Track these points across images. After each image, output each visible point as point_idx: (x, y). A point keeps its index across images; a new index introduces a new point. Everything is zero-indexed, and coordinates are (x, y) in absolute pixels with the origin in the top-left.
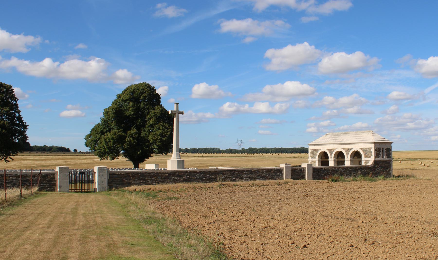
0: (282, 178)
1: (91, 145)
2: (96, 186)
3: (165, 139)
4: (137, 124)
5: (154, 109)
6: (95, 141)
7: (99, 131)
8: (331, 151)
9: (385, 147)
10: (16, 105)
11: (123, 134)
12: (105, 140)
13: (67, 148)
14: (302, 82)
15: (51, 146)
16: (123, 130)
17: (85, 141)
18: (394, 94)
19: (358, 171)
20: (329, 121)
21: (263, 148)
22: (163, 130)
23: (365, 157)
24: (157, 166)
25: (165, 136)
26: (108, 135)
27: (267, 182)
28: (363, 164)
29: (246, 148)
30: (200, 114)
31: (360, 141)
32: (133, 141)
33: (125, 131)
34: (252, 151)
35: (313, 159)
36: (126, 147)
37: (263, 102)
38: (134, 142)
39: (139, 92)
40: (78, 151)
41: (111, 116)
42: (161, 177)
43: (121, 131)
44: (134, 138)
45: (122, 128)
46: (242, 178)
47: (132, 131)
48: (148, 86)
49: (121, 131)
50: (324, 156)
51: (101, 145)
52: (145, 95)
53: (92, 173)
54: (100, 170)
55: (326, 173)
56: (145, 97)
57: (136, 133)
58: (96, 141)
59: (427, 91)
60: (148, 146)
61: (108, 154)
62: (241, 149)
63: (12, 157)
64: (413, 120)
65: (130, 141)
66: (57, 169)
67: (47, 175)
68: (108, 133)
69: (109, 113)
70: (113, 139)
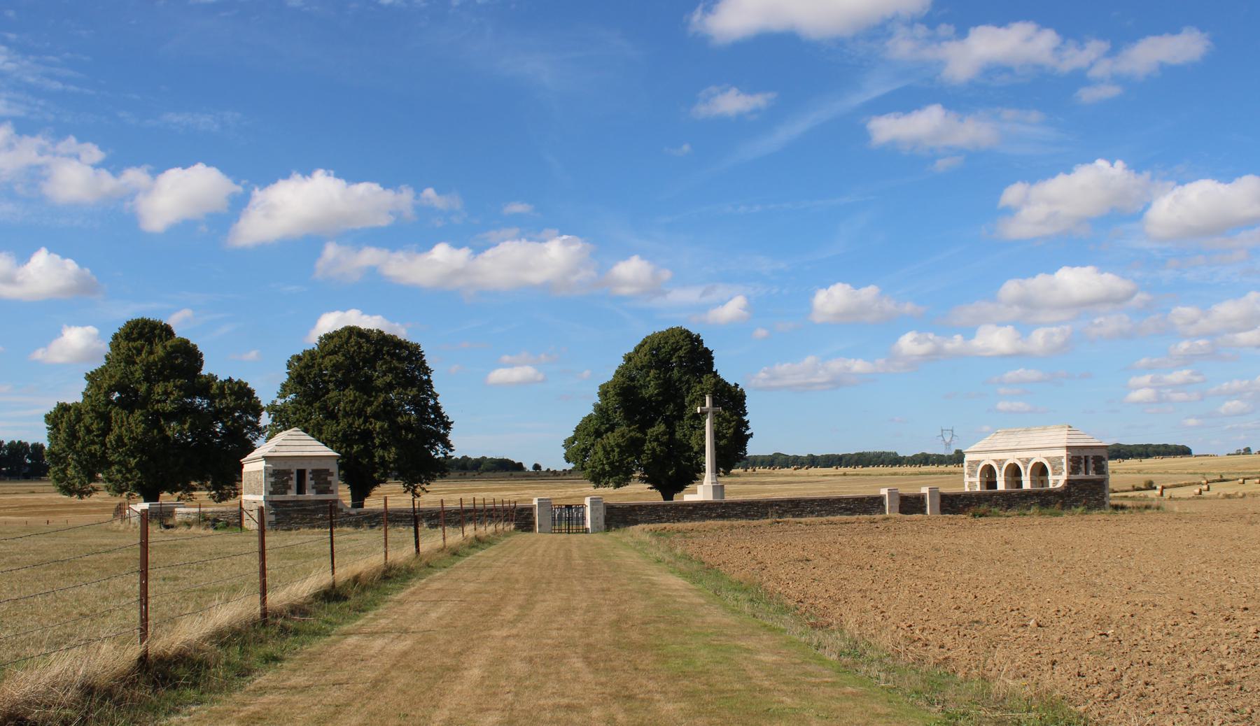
0: (883, 511)
2: (588, 525)
4: (666, 415)
5: (700, 382)
6: (583, 450)
8: (1000, 462)
9: (1091, 454)
10: (429, 382)
11: (639, 435)
12: (604, 448)
13: (516, 461)
14: (1102, 267)
15: (479, 456)
19: (1045, 500)
20: (1186, 372)
23: (1054, 474)
25: (724, 436)
27: (854, 518)
28: (1051, 486)
30: (836, 365)
31: (1043, 446)
32: (658, 449)
33: (643, 429)
35: (973, 479)
37: (1001, 324)
39: (668, 348)
40: (544, 469)
41: (613, 401)
42: (682, 511)
45: (636, 422)
46: (812, 512)
48: (688, 334)
50: (989, 472)
51: (596, 457)
52: (681, 353)
53: (583, 507)
54: (594, 502)
55: (965, 502)
56: (680, 357)
57: (664, 433)
58: (586, 450)
61: (611, 476)
62: (952, 452)
63: (424, 486)
65: (654, 449)
66: (535, 502)
67: (523, 510)
70: (618, 445)
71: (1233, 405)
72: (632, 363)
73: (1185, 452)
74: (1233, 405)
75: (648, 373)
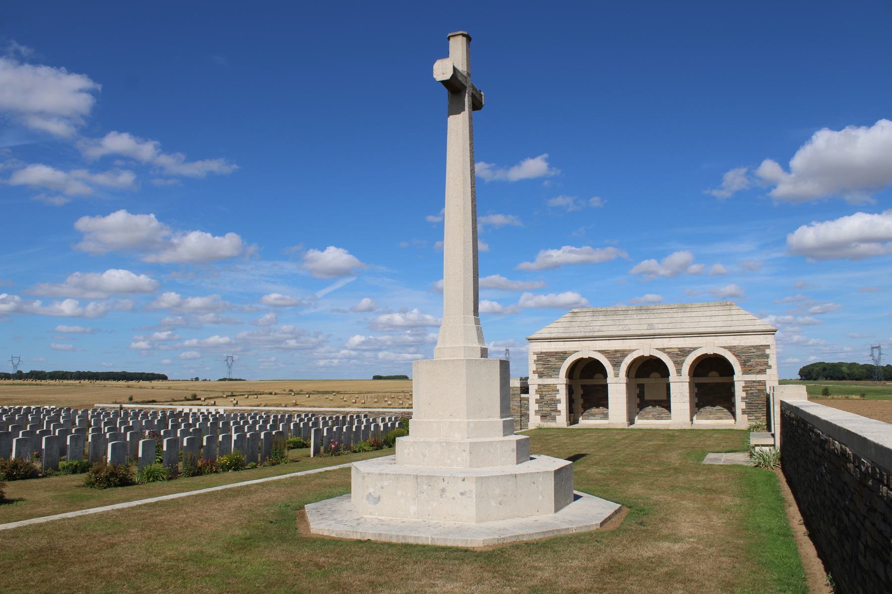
8: (616, 357)
23: (745, 372)
29: (26, 370)
59: (320, 294)
62: (15, 372)
64: (296, 335)
73: (164, 378)
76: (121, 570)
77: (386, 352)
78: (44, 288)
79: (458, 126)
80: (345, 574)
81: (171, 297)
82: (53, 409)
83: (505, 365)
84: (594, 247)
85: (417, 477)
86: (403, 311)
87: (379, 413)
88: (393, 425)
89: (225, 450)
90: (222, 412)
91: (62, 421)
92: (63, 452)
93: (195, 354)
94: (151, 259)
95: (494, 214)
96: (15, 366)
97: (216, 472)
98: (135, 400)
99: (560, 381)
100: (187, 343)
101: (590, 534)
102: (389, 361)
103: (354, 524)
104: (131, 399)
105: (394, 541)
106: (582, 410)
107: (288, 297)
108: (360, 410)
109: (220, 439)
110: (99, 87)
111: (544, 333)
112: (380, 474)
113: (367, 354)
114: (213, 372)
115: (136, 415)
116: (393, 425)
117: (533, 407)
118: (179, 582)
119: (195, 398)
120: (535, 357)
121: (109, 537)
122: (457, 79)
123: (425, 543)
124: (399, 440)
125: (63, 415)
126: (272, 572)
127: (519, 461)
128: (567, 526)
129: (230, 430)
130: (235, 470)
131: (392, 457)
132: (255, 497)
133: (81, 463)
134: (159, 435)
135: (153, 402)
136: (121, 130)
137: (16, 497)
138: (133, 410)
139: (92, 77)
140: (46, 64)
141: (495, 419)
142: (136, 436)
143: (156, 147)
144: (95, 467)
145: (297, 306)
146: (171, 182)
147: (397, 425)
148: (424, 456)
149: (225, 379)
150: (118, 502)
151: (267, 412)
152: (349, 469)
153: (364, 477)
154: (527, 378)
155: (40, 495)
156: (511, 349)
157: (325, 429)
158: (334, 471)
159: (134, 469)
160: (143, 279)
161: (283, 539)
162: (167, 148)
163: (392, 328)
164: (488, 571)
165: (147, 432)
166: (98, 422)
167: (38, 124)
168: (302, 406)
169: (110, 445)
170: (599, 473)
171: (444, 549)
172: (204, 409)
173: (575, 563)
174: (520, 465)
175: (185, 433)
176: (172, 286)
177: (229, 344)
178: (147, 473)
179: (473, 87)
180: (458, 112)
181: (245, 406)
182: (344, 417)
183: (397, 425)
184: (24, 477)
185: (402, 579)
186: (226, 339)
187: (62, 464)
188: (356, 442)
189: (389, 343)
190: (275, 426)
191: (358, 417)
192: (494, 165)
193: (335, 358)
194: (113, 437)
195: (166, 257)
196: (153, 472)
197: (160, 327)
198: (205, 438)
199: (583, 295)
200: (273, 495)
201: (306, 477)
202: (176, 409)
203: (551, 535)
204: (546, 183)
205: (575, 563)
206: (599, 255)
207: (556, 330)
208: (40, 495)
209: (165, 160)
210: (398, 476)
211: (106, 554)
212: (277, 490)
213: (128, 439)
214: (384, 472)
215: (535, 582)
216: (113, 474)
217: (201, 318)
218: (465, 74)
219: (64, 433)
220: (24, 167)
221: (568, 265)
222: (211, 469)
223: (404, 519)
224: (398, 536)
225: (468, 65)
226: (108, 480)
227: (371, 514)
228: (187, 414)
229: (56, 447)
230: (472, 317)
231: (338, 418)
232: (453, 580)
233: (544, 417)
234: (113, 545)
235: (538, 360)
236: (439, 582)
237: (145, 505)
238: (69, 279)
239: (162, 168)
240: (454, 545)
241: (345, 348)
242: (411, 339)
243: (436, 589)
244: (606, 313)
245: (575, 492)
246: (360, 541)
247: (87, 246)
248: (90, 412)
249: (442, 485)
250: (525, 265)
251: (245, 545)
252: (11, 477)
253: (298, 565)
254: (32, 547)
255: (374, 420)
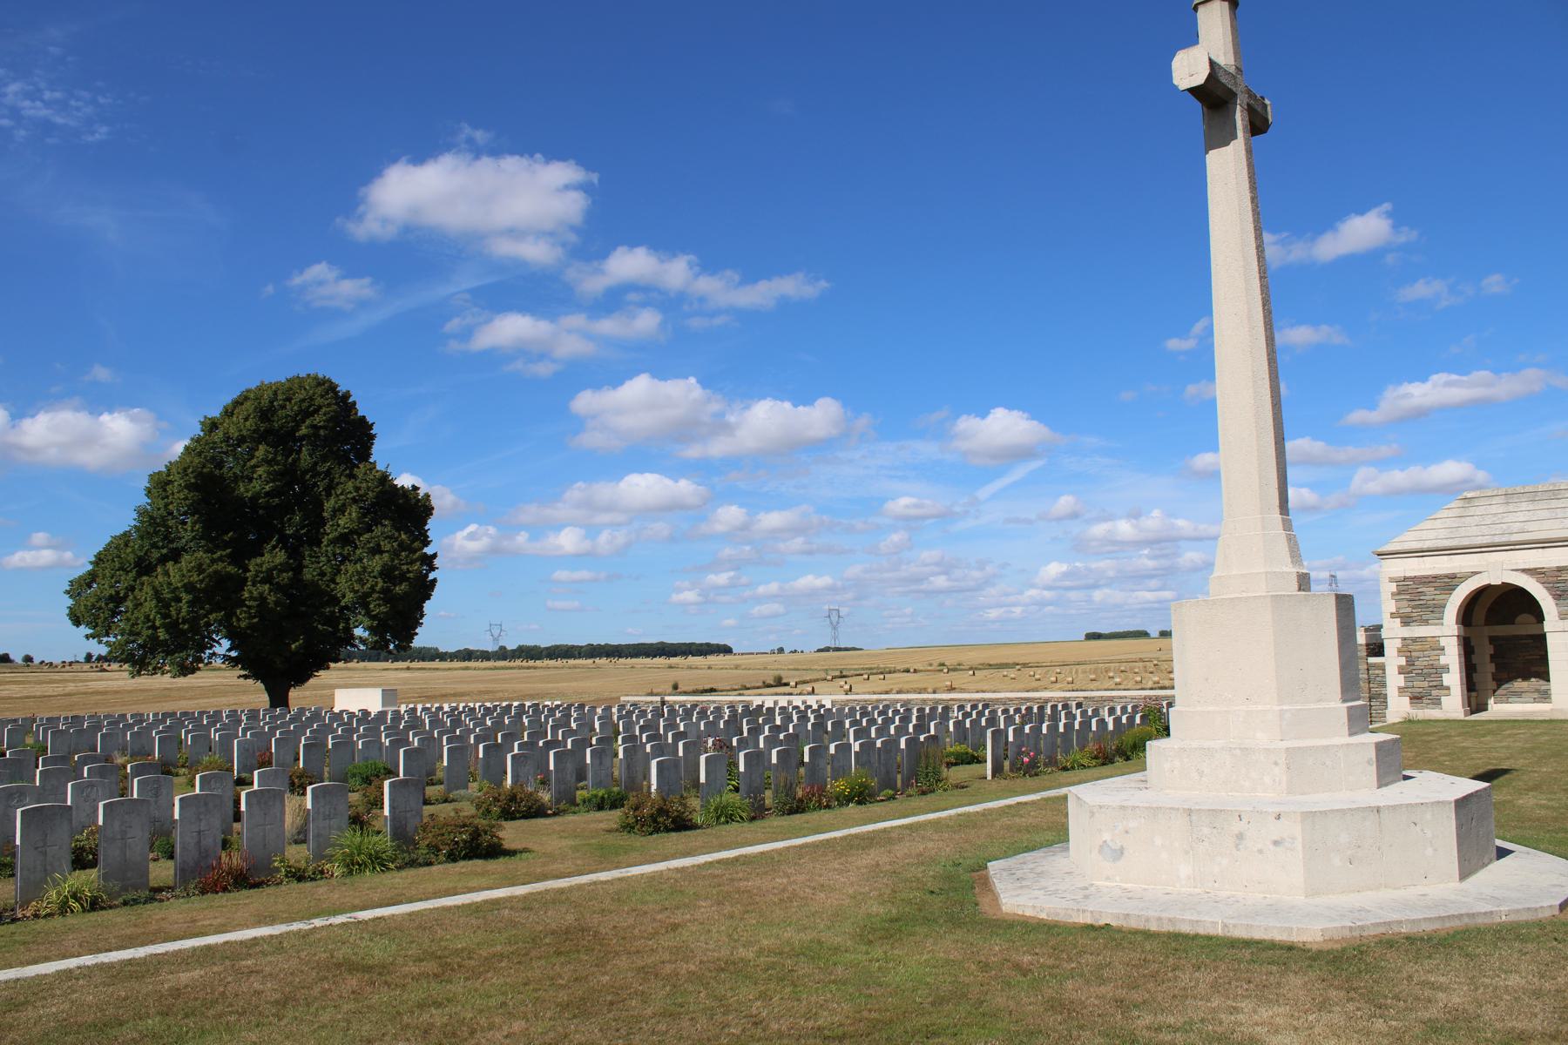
1: (97, 617)
3: (400, 589)
6: (111, 598)
7: (131, 558)
11: (231, 569)
12: (157, 594)
16: (228, 556)
17: (70, 602)
18: (902, 504)
21: (557, 647)
22: (395, 554)
24: (389, 696)
25: (403, 578)
26: (167, 573)
29: (511, 646)
32: (271, 599)
33: (239, 558)
34: (529, 653)
36: (243, 625)
38: (277, 603)
39: (292, 409)
41: (180, 496)
43: (221, 559)
44: (277, 588)
45: (226, 545)
47: (267, 557)
49: (221, 559)
52: (318, 419)
57: (284, 568)
58: (117, 600)
59: (983, 493)
60: (332, 621)
61: (168, 653)
62: (496, 648)
64: (946, 568)
65: (262, 599)
68: (170, 565)
69: (169, 488)
70: (189, 588)
71: (766, 609)
72: (218, 435)
73: (727, 650)
74: (766, 609)
75: (254, 449)
76: (693, 968)
77: (1107, 591)
78: (530, 513)
79: (1226, 169)
80: (1069, 984)
81: (731, 514)
82: (558, 707)
83: (1345, 604)
84: (1496, 371)
85: (1189, 812)
86: (1135, 515)
87: (1103, 700)
88: (1131, 719)
89: (841, 771)
90: (829, 706)
91: (574, 725)
92: (581, 775)
93: (776, 607)
94: (693, 452)
95: (1292, 326)
96: (496, 640)
97: (828, 807)
98: (682, 688)
99: (1447, 631)
100: (761, 589)
101: (1540, 924)
102: (1119, 605)
103: (1079, 897)
104: (675, 687)
105: (1154, 927)
106: (1493, 685)
107: (927, 502)
108: (1068, 694)
109: (832, 750)
110: (595, 178)
111: (1409, 540)
112: (1123, 808)
113: (1073, 595)
114: (808, 637)
115: (688, 713)
116: (1131, 719)
117: (1394, 680)
118: (788, 990)
119: (779, 682)
120: (1393, 587)
121: (667, 913)
122: (1218, 81)
123: (1212, 932)
124: (1153, 746)
125: (575, 715)
126: (941, 978)
127: (1382, 782)
128: (1488, 908)
129: (845, 735)
130: (859, 803)
131: (1139, 776)
132: (900, 850)
133: (609, 793)
134: (730, 747)
135: (712, 690)
136: (633, 244)
137: (519, 847)
138: (682, 705)
139: (584, 163)
140: (512, 152)
141: (1332, 705)
142: (694, 748)
143: (691, 265)
144: (632, 800)
145: (946, 516)
146: (718, 321)
147: (1138, 720)
148: (1201, 774)
149: (827, 649)
150: (674, 857)
151: (906, 703)
152: (1065, 798)
153: (1092, 814)
154: (1379, 628)
155: (554, 844)
156: (1339, 575)
157: (1011, 730)
158: (1033, 803)
159: (695, 803)
160: (685, 488)
161: (955, 922)
162: (708, 266)
163: (1116, 546)
164: (1337, 988)
165: (710, 741)
166: (629, 726)
167: (505, 248)
168: (963, 690)
169: (654, 763)
170: (1542, 807)
171: (1247, 943)
172: (798, 701)
173: (1514, 980)
174: (1384, 789)
175: (772, 741)
176: (731, 496)
177: (832, 589)
178: (716, 810)
179: (1249, 92)
180: (1226, 138)
181: (865, 693)
182: (1041, 708)
183: (1138, 720)
184: (528, 815)
185: (1174, 996)
186: (825, 581)
187: (581, 795)
188: (1067, 752)
189: (1111, 574)
190: (921, 727)
191: (1065, 706)
192: (1285, 234)
193: (1014, 605)
194: (659, 750)
195: (718, 448)
196: (725, 807)
197: (716, 565)
198: (806, 749)
199: (1479, 465)
200: (930, 845)
201: (984, 814)
202: (750, 703)
203: (1456, 924)
204: (1390, 259)
205: (1514, 980)
206: (1506, 387)
207: (1432, 534)
208: (554, 844)
209: (707, 285)
210: (1154, 811)
211: (667, 941)
212: (936, 837)
213: (681, 754)
214: (1129, 804)
215: (1433, 1012)
216: (661, 811)
217: (781, 546)
218: (1232, 70)
219: (581, 744)
220: (488, 321)
221: (1445, 410)
222: (820, 801)
223: (1169, 889)
224: (1159, 919)
225: (1236, 53)
226: (655, 821)
227: (1108, 878)
228: (771, 711)
229: (570, 767)
230: (1277, 517)
231: (1029, 709)
232: (1271, 1001)
233: (1416, 699)
234: (675, 927)
235: (1399, 593)
236: (1246, 1005)
237: (719, 862)
238: (568, 495)
239: (702, 299)
240: (1267, 936)
241: (1033, 586)
242: (1151, 564)
243: (1240, 1017)
244: (1534, 497)
245: (1499, 843)
246: (1091, 928)
247: (592, 439)
248: (614, 710)
249: (1237, 827)
250: (1358, 416)
251: (891, 930)
252: (508, 815)
253: (985, 967)
254: (554, 926)
255: (1096, 712)
